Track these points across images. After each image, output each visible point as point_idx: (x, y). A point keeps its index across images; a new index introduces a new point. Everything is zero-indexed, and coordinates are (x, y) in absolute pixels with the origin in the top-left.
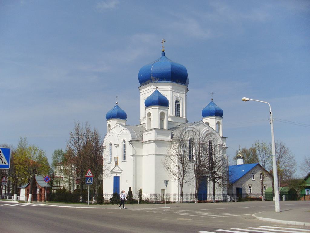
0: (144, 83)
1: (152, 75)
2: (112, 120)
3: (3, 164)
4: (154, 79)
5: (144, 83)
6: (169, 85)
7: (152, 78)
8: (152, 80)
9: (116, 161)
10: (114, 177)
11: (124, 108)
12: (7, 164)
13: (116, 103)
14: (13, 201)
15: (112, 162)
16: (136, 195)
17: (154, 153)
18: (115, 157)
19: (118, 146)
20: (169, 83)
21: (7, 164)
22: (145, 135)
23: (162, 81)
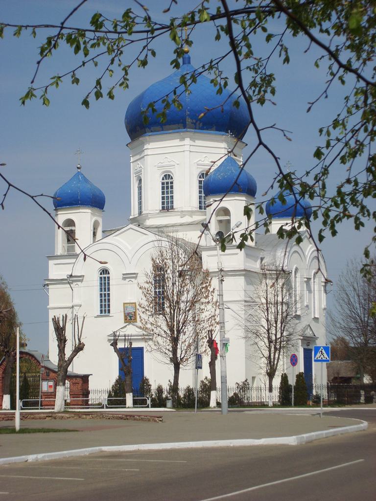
0: (161, 129)
1: (189, 115)
2: (81, 210)
3: (325, 359)
4: (192, 123)
5: (158, 128)
6: (222, 141)
7: (189, 121)
8: (188, 126)
9: (128, 314)
10: (143, 348)
11: (99, 182)
12: (328, 359)
13: (78, 168)
14: (129, 408)
15: (111, 315)
16: (321, 387)
17: (243, 298)
18: (124, 304)
19: (136, 278)
20: (224, 136)
21: (328, 359)
22: (209, 256)
23: (207, 129)
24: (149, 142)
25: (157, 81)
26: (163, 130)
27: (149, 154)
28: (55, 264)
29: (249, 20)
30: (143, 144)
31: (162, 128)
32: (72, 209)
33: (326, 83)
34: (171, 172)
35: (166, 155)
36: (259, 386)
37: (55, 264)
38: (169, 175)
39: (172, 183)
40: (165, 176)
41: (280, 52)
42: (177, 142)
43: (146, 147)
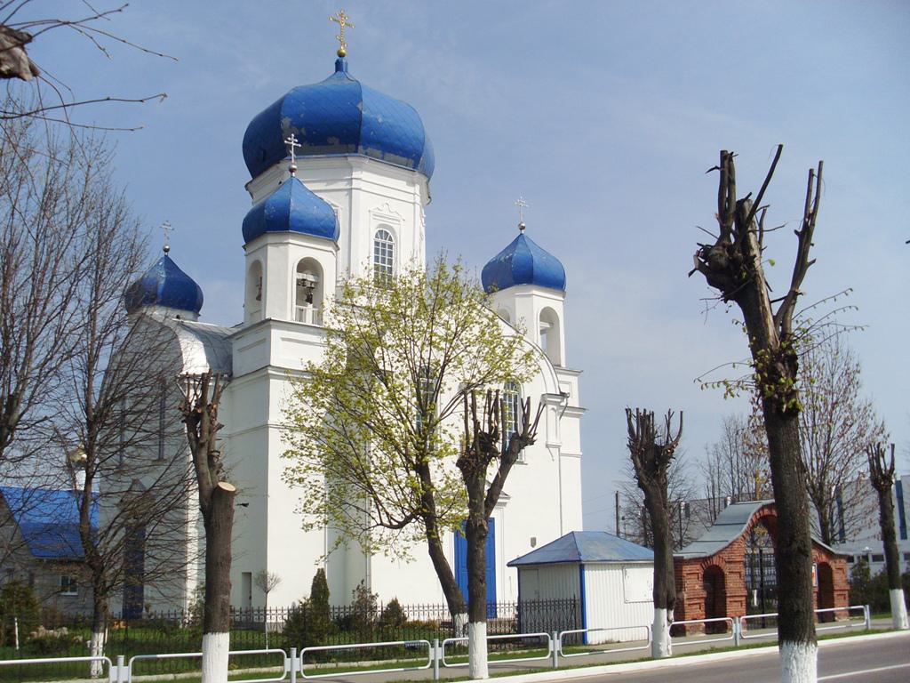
0: (381, 155)
5: (378, 153)
24: (361, 168)
25: (422, 119)
26: (383, 158)
27: (363, 189)
28: (283, 339)
29: (759, 547)
30: (351, 168)
31: (384, 154)
32: (309, 239)
33: (529, 398)
34: (394, 232)
35: (388, 201)
36: (573, 598)
37: (283, 339)
38: (387, 234)
39: (390, 247)
40: (381, 232)
41: (679, 436)
42: (402, 185)
43: (355, 175)
